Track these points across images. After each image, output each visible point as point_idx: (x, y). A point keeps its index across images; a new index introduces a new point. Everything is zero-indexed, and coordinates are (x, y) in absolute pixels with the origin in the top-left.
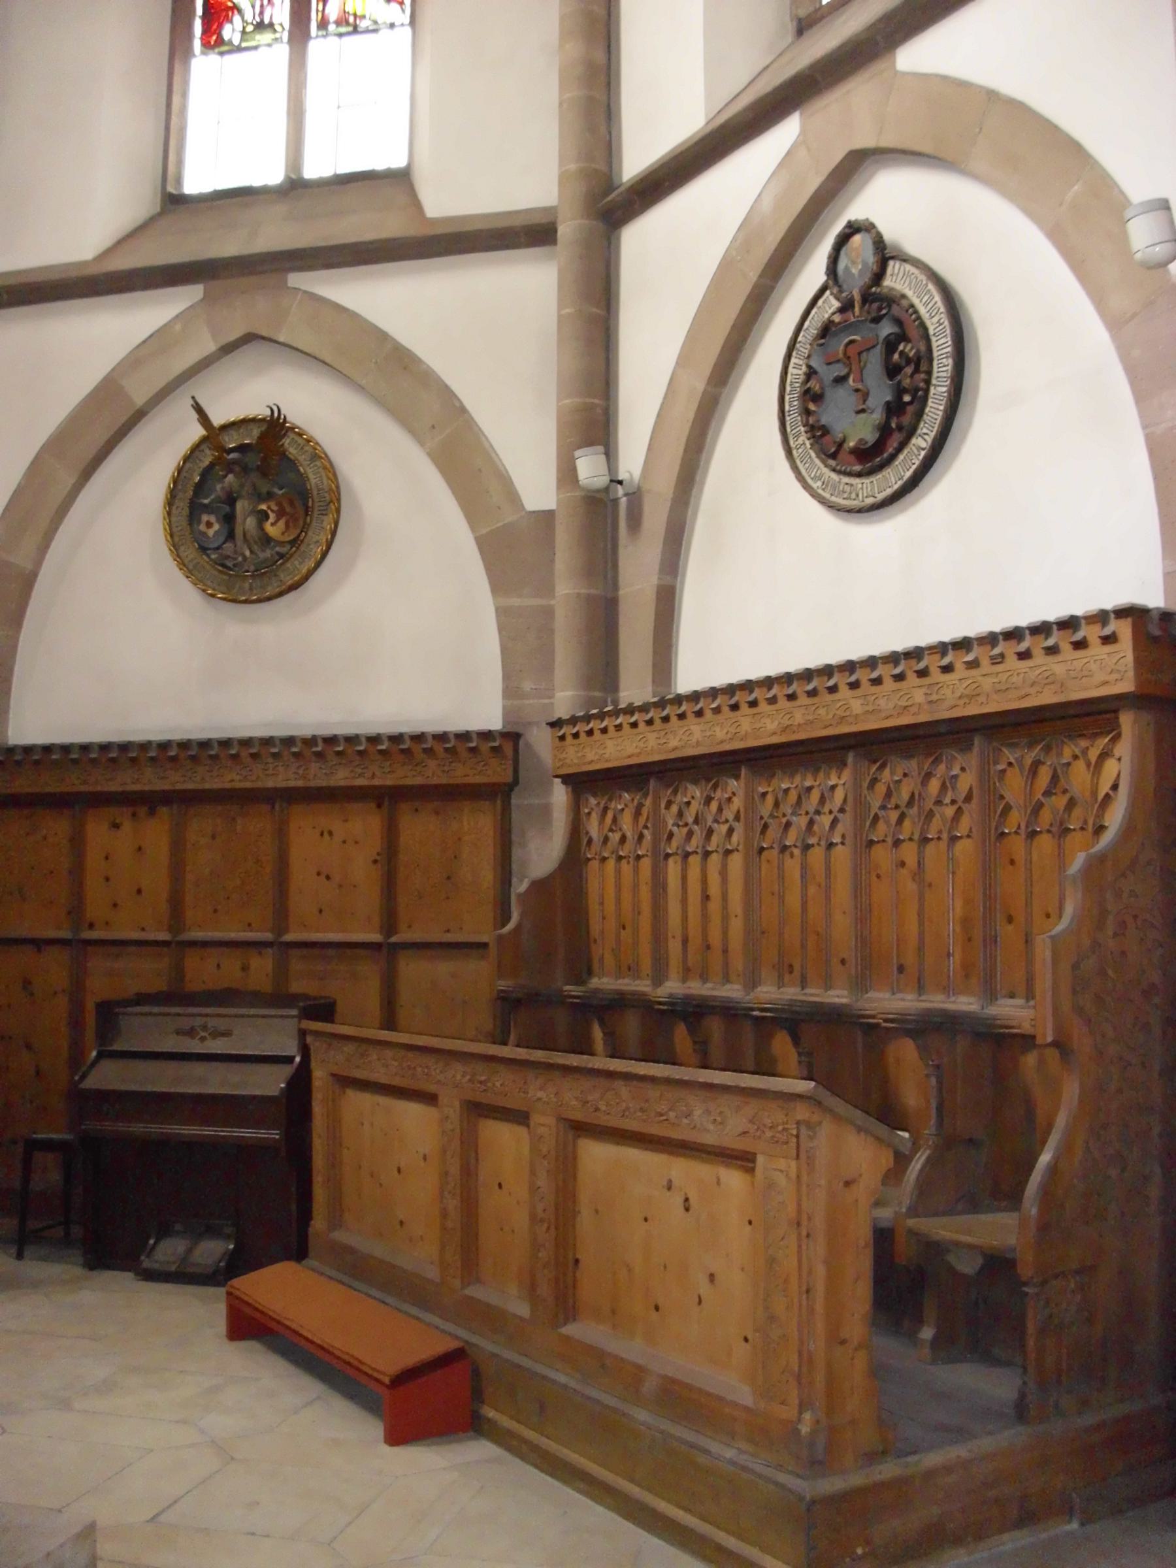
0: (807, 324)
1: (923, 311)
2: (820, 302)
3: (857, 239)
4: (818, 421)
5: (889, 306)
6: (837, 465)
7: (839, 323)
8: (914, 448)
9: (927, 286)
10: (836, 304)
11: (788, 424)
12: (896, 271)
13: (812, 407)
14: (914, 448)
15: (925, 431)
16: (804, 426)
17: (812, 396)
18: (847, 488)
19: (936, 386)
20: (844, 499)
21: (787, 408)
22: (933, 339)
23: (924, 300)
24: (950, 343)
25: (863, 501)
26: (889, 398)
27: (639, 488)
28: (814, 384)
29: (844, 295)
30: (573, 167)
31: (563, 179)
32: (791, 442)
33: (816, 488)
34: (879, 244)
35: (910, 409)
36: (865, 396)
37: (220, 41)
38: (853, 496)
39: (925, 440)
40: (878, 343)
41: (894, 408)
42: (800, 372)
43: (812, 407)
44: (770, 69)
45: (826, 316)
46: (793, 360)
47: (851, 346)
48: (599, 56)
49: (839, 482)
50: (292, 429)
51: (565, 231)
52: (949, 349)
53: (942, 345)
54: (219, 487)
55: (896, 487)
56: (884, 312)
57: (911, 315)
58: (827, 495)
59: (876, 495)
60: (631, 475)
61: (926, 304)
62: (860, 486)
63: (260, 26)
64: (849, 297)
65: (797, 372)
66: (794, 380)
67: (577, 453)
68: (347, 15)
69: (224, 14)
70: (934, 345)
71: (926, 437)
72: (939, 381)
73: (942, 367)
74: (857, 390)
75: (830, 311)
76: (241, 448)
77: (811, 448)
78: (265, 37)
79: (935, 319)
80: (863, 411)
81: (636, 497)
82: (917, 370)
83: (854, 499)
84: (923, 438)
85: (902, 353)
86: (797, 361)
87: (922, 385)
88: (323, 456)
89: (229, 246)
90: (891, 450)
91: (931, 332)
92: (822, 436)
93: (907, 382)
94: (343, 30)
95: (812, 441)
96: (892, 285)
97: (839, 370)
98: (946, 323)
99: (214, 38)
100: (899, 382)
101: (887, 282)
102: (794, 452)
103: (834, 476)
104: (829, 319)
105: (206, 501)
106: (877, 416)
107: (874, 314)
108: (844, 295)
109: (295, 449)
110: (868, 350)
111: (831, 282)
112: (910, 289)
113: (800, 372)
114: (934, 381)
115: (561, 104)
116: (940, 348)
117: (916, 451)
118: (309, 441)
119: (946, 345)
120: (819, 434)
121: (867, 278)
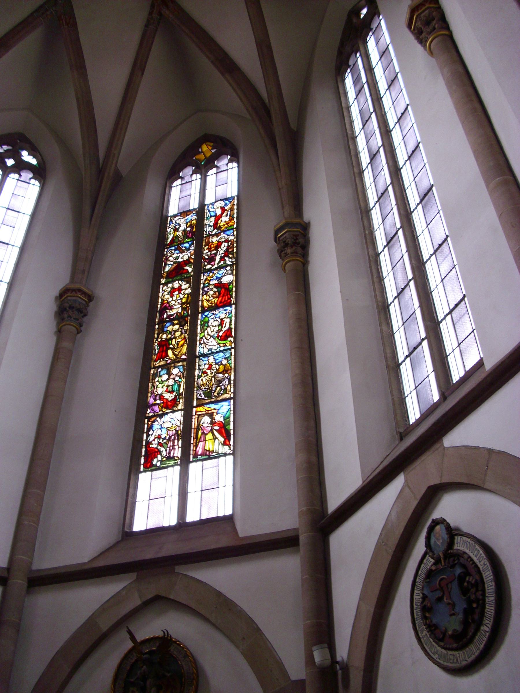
0: (420, 572)
1: (475, 559)
2: (425, 561)
3: (438, 527)
4: (431, 621)
5: (458, 559)
6: (444, 645)
7: (435, 570)
8: (482, 632)
9: (475, 546)
10: (432, 561)
11: (417, 625)
12: (459, 541)
13: (427, 615)
14: (482, 632)
15: (487, 622)
16: (425, 626)
17: (425, 609)
18: (451, 657)
19: (488, 597)
20: (451, 663)
21: (415, 616)
22: (483, 573)
23: (475, 554)
24: (491, 574)
25: (461, 663)
26: (465, 606)
27: (347, 665)
28: (427, 603)
29: (435, 556)
30: (304, 509)
31: (301, 514)
32: (420, 634)
33: (435, 658)
34: (448, 528)
35: (478, 611)
36: (453, 605)
37: (152, 465)
38: (455, 661)
39: (488, 627)
40: (455, 578)
41: (468, 612)
42: (419, 597)
43: (427, 615)
44: (389, 456)
45: (428, 567)
46: (416, 591)
47: (441, 582)
48: (314, 459)
49: (447, 654)
50: (175, 642)
51: (303, 538)
52: (492, 577)
53: (488, 575)
54: (139, 672)
55: (477, 654)
56: (456, 562)
57: (470, 562)
58: (442, 662)
59: (468, 660)
60: (343, 658)
61: (476, 556)
62: (458, 655)
63: (169, 458)
64: (438, 556)
65: (418, 597)
66: (417, 602)
67: (314, 648)
68: (206, 451)
69: (154, 454)
70: (484, 576)
71: (488, 625)
72: (489, 595)
73: (490, 587)
74: (449, 604)
75: (430, 565)
76: (151, 653)
77: (430, 637)
78: (171, 463)
79: (482, 563)
80: (454, 614)
81: (345, 668)
82: (477, 590)
83: (456, 663)
84: (487, 626)
85: (468, 582)
86: (417, 592)
87: (481, 597)
88: (190, 655)
89: (149, 554)
90: (470, 634)
91: (481, 569)
92: (435, 630)
93: (473, 597)
94: (204, 457)
95: (430, 633)
96: (458, 548)
97: (439, 594)
98: (488, 564)
99: (149, 464)
100: (469, 597)
101: (456, 547)
102: (422, 640)
103: (444, 651)
104: (430, 569)
105: (132, 680)
106: (461, 617)
107: (451, 564)
108: (435, 556)
109: (177, 652)
110: (451, 582)
111: (428, 551)
112: (467, 549)
113: (419, 597)
114: (487, 595)
115: (297, 481)
116: (487, 577)
117: (484, 633)
118: (183, 648)
119: (490, 575)
120: (433, 629)
121: (445, 547)
